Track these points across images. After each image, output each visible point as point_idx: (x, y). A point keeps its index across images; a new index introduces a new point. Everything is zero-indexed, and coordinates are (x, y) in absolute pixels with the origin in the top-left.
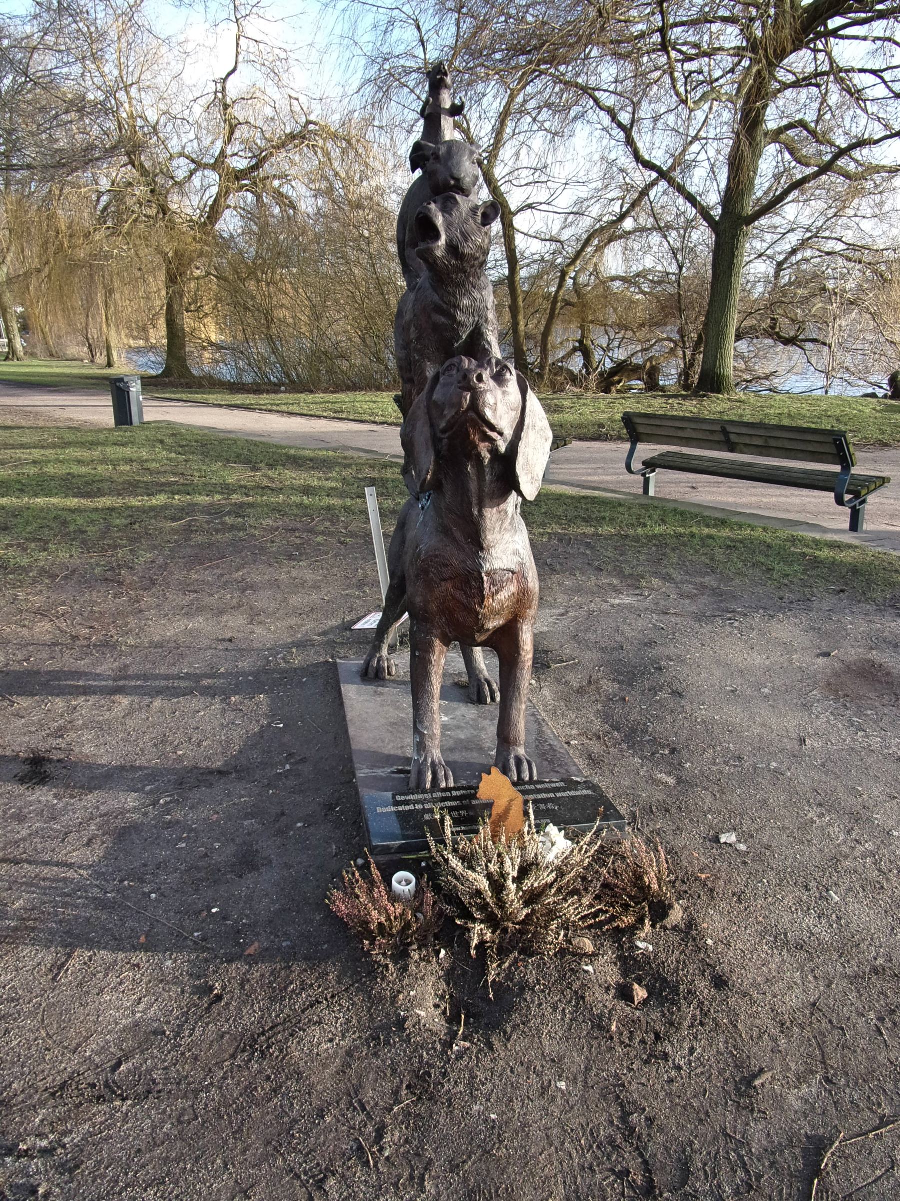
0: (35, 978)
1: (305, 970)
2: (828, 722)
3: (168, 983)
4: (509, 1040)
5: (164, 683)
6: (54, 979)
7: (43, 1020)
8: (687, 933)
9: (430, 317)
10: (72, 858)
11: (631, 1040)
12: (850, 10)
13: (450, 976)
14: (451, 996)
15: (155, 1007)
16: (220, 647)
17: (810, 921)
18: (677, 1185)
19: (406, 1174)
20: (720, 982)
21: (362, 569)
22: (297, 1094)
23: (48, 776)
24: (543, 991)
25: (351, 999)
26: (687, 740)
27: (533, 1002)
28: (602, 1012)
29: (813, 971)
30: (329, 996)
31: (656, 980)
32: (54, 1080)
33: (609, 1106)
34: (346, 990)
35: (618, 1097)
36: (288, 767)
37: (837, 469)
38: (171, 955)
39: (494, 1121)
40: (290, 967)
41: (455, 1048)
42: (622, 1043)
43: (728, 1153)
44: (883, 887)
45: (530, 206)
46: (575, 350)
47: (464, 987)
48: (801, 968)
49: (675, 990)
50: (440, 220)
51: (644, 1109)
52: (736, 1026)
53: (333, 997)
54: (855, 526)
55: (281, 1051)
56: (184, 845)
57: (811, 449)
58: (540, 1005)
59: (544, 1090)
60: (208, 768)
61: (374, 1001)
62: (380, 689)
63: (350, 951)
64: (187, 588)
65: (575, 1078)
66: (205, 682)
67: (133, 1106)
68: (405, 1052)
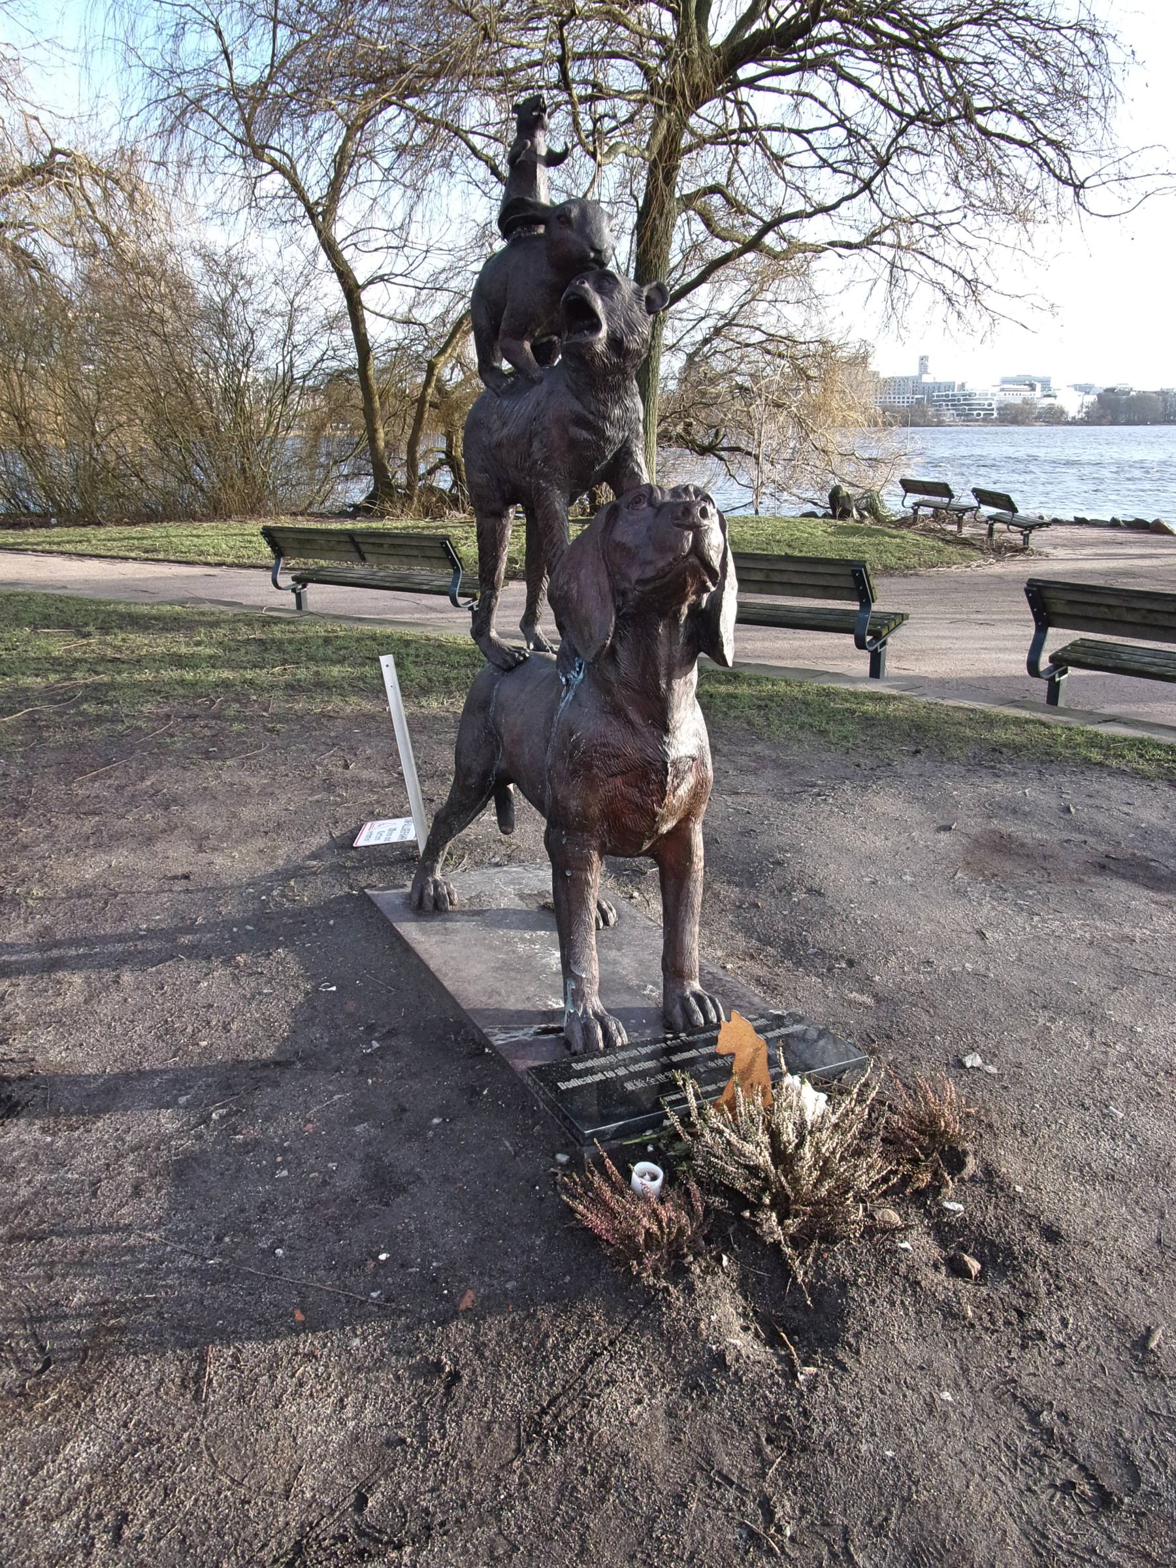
0: (166, 1403)
1: (556, 1316)
2: (994, 908)
3: (369, 1370)
4: (857, 1352)
5: (119, 947)
6: (197, 1397)
7: (215, 1462)
8: (991, 1183)
9: (566, 431)
10: (122, 1216)
11: (993, 1323)
12: (768, 57)
13: (744, 1287)
14: (755, 1313)
15: (369, 1409)
16: (176, 888)
17: (1106, 1145)
18: (1131, 1485)
19: (825, 1552)
20: (1052, 1235)
21: (320, 764)
22: (634, 1483)
23: (17, 1104)
24: (868, 1284)
25: (637, 1341)
26: (860, 947)
27: (862, 1299)
28: (947, 1296)
29: (1137, 1203)
30: (607, 1343)
31: (983, 1245)
32: (280, 1545)
33: (1010, 1409)
34: (625, 1330)
35: (1014, 1396)
36: (375, 1044)
37: (855, 606)
38: (354, 1330)
39: (893, 1459)
40: (534, 1315)
41: (801, 1378)
42: (987, 1329)
43: (1163, 1434)
44: (1159, 1094)
45: (381, 278)
46: (441, 463)
47: (764, 1298)
48: (1124, 1202)
49: (1010, 1254)
50: (599, 305)
51: (1051, 1404)
52: (1095, 1283)
53: (612, 1343)
54: (876, 671)
55: (582, 1430)
56: (285, 1173)
57: (822, 582)
58: (873, 1302)
59: (930, 1407)
60: (256, 1059)
61: (670, 1338)
62: (449, 924)
63: (609, 1277)
64: (79, 809)
65: (957, 1385)
66: (185, 940)
67: (417, 1552)
68: (741, 1395)
